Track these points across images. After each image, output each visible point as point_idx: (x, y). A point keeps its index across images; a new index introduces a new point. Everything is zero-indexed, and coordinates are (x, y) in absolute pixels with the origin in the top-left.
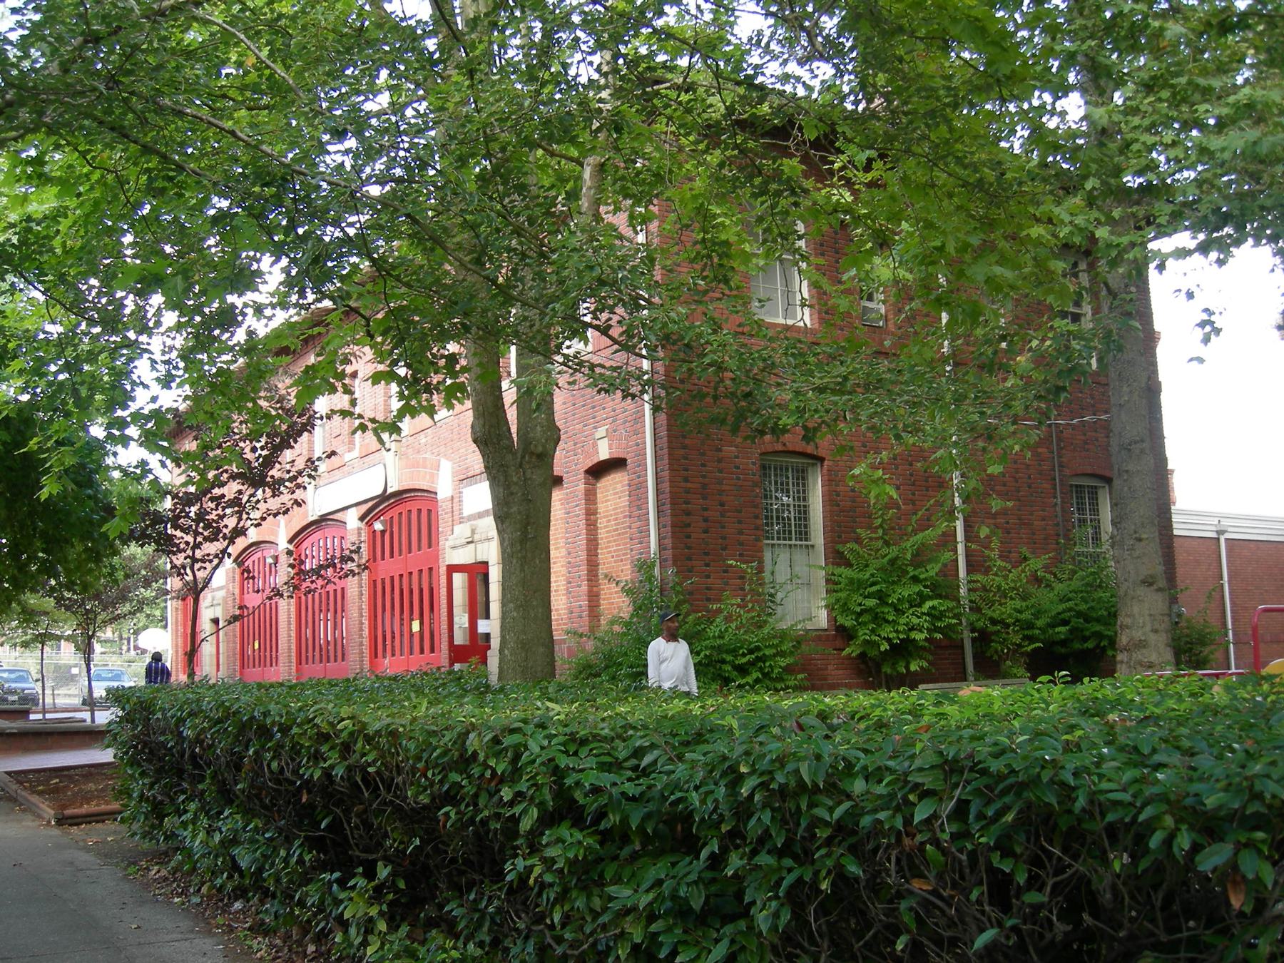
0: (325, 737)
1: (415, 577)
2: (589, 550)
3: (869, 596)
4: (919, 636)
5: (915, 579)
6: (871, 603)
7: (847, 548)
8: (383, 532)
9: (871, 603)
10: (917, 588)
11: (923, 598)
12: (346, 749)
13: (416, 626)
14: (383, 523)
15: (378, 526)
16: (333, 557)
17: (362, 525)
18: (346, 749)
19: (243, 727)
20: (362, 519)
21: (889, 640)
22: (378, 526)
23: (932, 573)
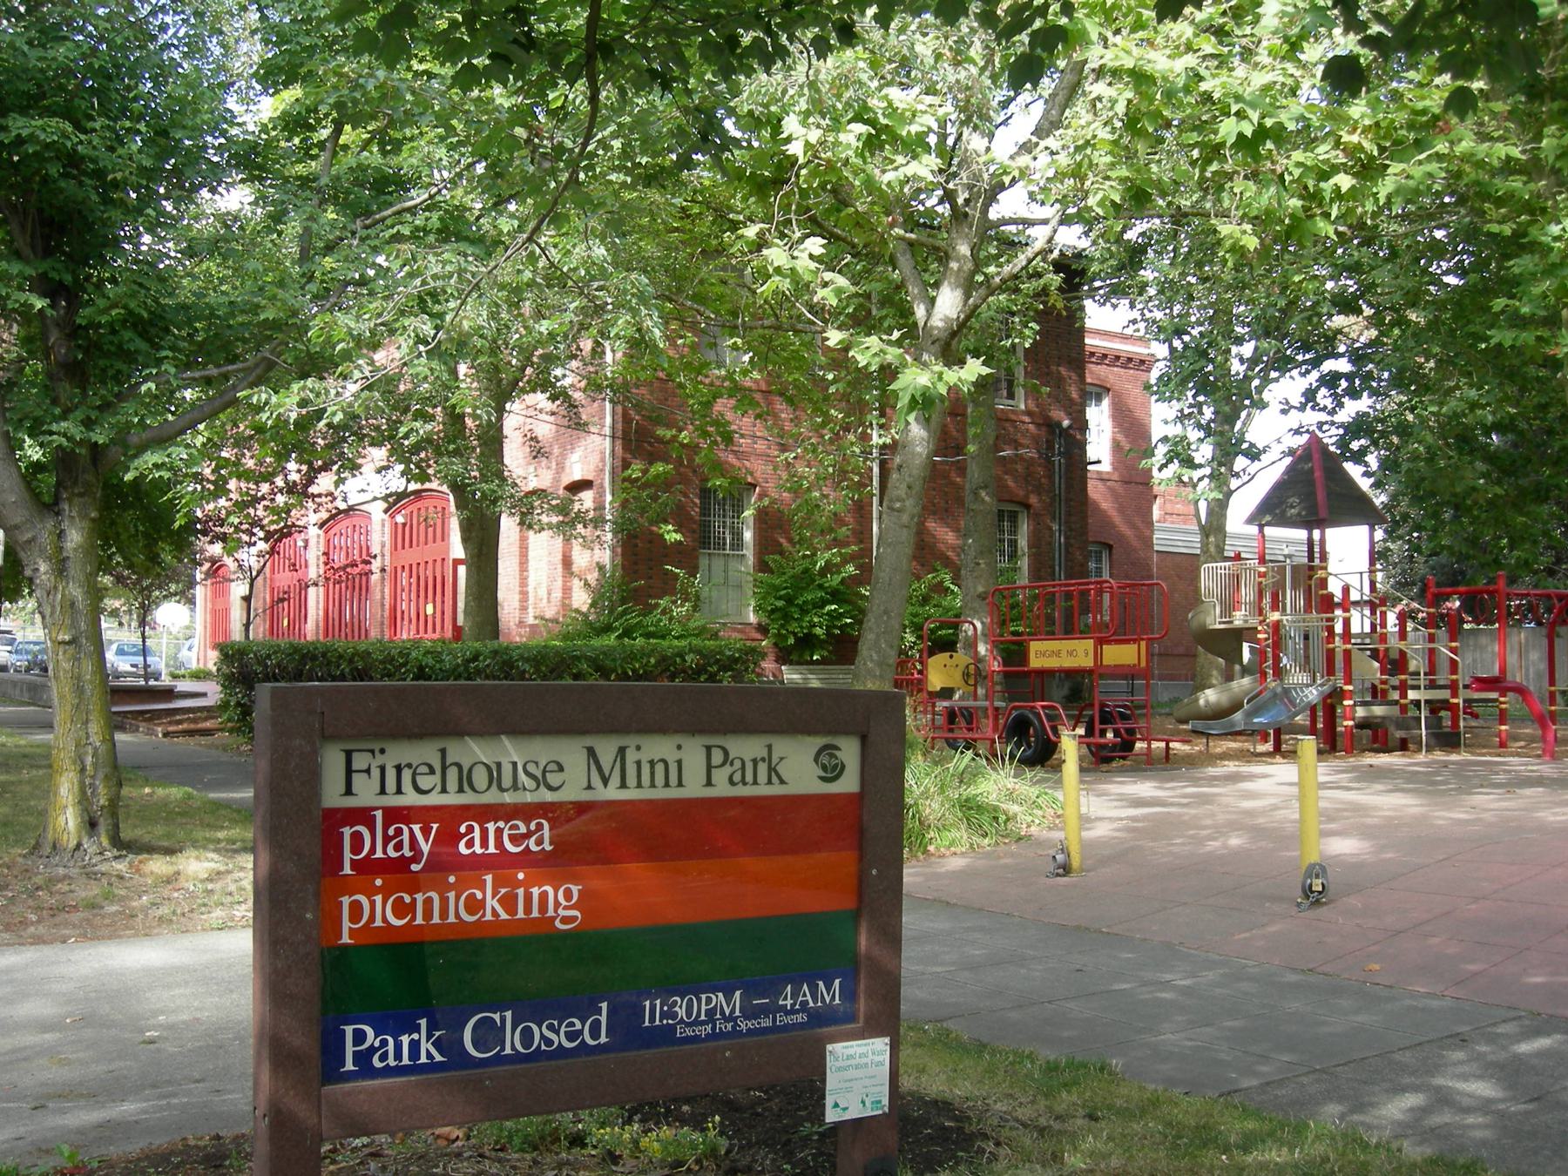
0: (341, 657)
1: (430, 565)
2: (527, 561)
3: (780, 598)
4: (818, 631)
5: (821, 587)
6: (780, 603)
7: (770, 558)
8: (404, 525)
9: (780, 603)
10: (820, 594)
11: (824, 603)
12: (351, 661)
13: (430, 609)
14: (405, 516)
15: (400, 519)
16: (59, 1053)
17: (386, 517)
18: (351, 661)
19: (304, 657)
20: (386, 511)
21: (795, 634)
22: (400, 519)
23: (834, 583)
